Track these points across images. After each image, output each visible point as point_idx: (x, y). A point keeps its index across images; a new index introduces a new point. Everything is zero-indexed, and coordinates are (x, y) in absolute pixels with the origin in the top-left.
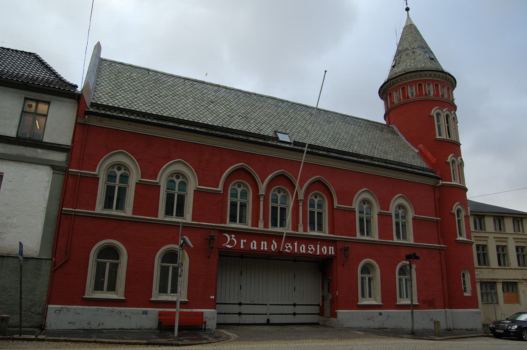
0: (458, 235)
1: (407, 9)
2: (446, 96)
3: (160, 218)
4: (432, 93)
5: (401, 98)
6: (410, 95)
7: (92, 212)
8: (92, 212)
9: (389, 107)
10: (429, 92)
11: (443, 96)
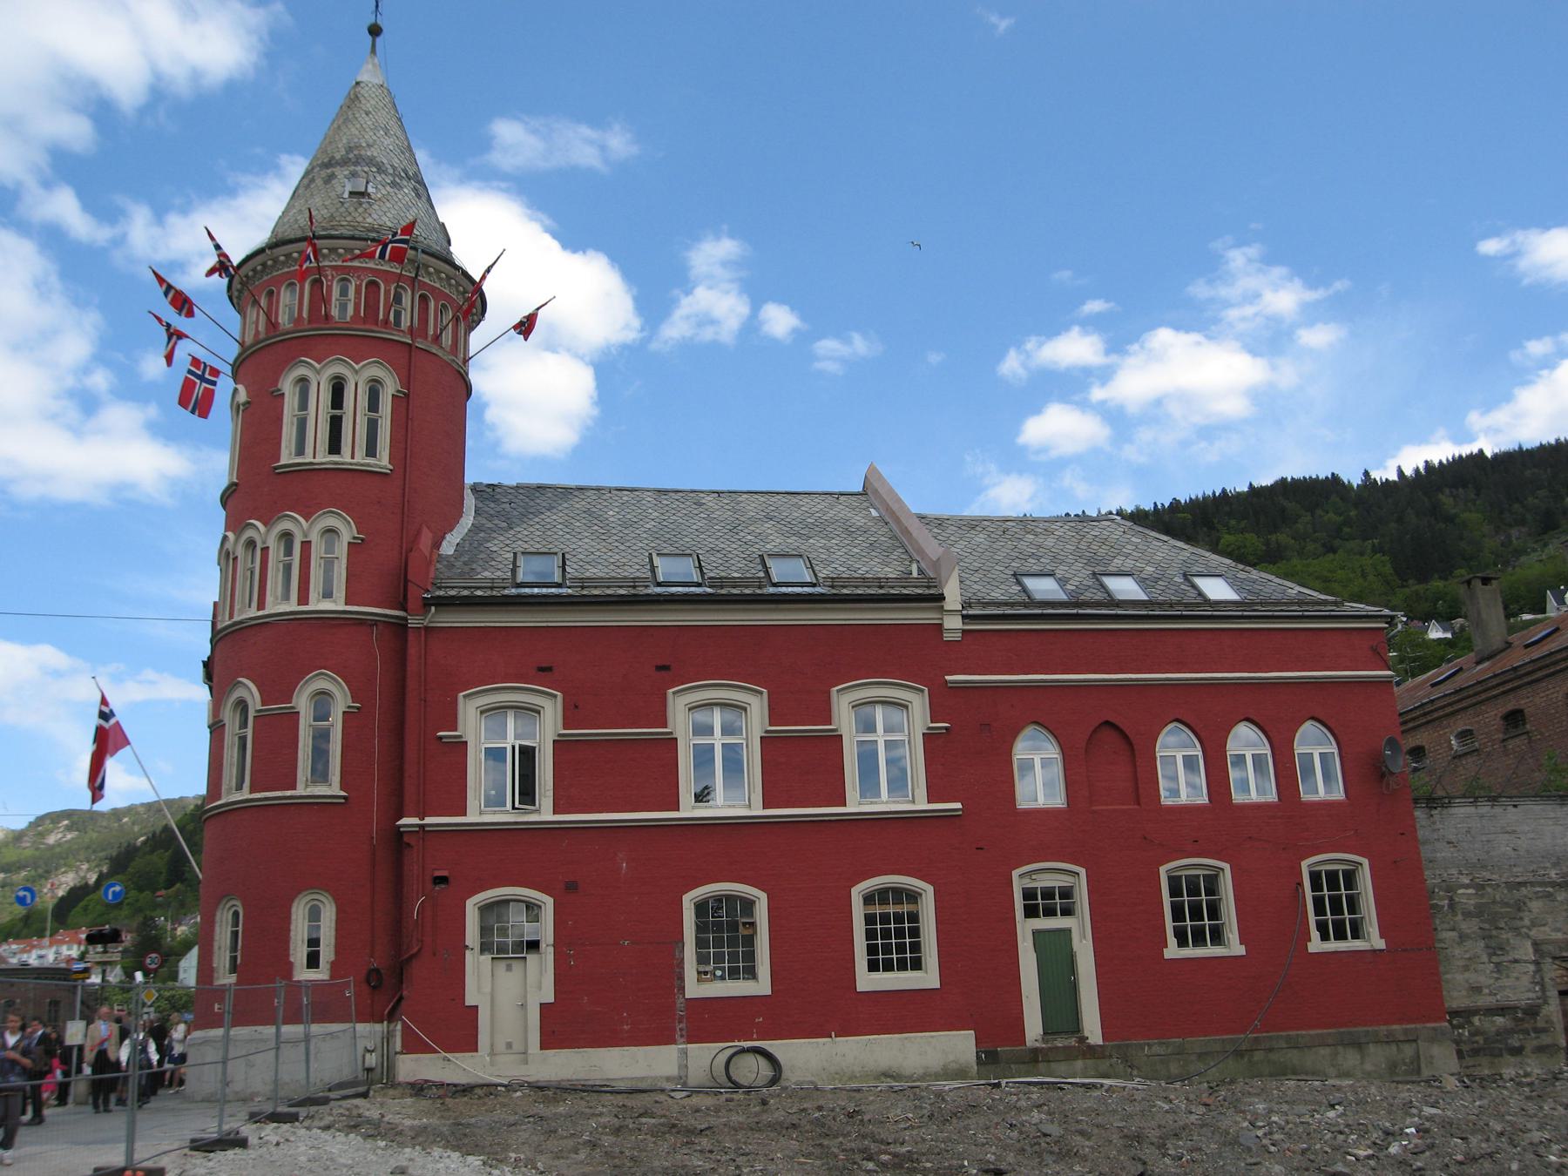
0: (1315, 934)
1: (375, 31)
2: (447, 339)
3: (300, 791)
4: (405, 322)
5: (305, 315)
6: (335, 312)
7: (289, 793)
8: (289, 793)
9: (262, 336)
10: (398, 315)
11: (437, 338)
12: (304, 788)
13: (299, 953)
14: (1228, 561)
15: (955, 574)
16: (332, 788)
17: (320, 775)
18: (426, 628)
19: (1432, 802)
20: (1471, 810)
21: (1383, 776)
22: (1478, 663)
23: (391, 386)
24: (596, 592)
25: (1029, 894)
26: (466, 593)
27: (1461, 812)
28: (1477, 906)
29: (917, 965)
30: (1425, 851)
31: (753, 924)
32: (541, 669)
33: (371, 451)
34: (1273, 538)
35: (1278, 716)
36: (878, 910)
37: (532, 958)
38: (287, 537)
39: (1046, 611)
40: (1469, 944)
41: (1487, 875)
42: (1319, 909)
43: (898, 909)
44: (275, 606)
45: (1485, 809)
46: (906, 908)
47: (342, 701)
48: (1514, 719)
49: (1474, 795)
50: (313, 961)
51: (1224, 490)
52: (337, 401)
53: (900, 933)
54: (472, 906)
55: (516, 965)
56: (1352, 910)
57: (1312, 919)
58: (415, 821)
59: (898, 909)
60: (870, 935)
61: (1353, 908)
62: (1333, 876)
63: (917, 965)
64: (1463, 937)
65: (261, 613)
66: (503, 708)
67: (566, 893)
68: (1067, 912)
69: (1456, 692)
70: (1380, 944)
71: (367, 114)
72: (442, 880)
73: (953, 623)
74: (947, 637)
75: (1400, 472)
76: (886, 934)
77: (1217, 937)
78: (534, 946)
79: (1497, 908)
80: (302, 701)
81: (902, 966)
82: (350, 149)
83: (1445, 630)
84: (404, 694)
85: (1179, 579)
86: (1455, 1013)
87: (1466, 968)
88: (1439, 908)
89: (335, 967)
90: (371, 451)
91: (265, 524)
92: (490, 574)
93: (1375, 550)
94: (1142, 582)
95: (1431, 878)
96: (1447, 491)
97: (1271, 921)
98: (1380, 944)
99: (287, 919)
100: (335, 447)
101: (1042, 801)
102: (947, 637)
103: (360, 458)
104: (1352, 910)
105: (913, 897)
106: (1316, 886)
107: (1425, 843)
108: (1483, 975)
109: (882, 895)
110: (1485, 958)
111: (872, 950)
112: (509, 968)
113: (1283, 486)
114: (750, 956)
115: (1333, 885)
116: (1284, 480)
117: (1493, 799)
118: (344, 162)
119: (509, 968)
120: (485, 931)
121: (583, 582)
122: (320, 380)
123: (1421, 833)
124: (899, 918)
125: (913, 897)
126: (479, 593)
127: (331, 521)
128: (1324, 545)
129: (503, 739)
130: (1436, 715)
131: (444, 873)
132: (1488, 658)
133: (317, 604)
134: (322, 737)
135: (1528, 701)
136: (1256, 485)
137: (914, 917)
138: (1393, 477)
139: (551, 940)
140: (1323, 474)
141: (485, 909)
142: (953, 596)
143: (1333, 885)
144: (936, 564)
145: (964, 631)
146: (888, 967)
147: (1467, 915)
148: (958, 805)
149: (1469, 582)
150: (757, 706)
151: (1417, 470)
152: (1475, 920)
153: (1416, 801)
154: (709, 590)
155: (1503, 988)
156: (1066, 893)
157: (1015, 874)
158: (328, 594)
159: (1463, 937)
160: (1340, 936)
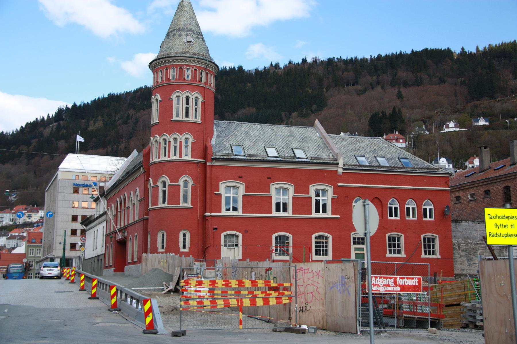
0: (423, 253)
7: (178, 206)
8: (178, 206)
11: (210, 85)
12: (182, 205)
13: (181, 245)
14: (410, 154)
15: (342, 158)
16: (189, 205)
17: (185, 201)
18: (212, 166)
19: (457, 221)
20: (467, 224)
21: (444, 215)
22: (480, 172)
23: (201, 99)
24: (254, 158)
25: (354, 239)
26: (222, 157)
27: (464, 224)
28: (466, 248)
29: (326, 254)
30: (453, 234)
31: (289, 243)
32: (240, 177)
33: (196, 117)
34: (419, 75)
35: (419, 197)
36: (318, 240)
37: (236, 248)
38: (175, 139)
39: (361, 167)
40: (462, 258)
41: (469, 241)
42: (425, 247)
43: (323, 241)
44: (173, 158)
45: (471, 224)
46: (324, 241)
47: (191, 183)
48: (487, 192)
49: (467, 221)
50: (184, 247)
51: (401, 52)
52: (187, 103)
53: (323, 247)
54: (223, 235)
55: (233, 250)
56: (433, 248)
57: (423, 249)
58: (209, 214)
59: (323, 241)
60: (316, 247)
61: (433, 247)
62: (429, 239)
63: (326, 254)
64: (461, 256)
65: (169, 159)
66: (230, 186)
67: (245, 233)
68: (363, 244)
69: (471, 182)
70: (439, 257)
71: (187, 13)
72: (216, 229)
73: (340, 171)
74: (339, 174)
76: (320, 247)
77: (399, 252)
78: (237, 245)
79: (471, 249)
80: (181, 183)
81: (323, 255)
82: (184, 26)
83: (486, 121)
84: (206, 182)
85: (397, 159)
86: (457, 275)
87: (461, 264)
88: (455, 248)
89: (190, 248)
90: (196, 117)
91: (169, 135)
92: (226, 152)
93: (462, 83)
94: (388, 160)
95: (454, 241)
96: (497, 59)
98: (439, 257)
99: (178, 236)
100: (187, 116)
102: (339, 174)
103: (194, 119)
104: (433, 248)
105: (327, 238)
106: (425, 241)
107: (454, 231)
108: (466, 267)
110: (466, 262)
111: (316, 250)
112: (230, 251)
113: (426, 52)
115: (429, 241)
116: (427, 49)
117: (473, 222)
118: (183, 30)
119: (230, 251)
120: (225, 241)
121: (250, 156)
122: (183, 96)
123: (453, 229)
125: (327, 238)
126: (225, 157)
127: (187, 136)
128: (440, 79)
129: (231, 194)
131: (216, 227)
132: (483, 171)
133: (184, 158)
134: (186, 192)
135: (491, 188)
136: (414, 50)
137: (326, 243)
138: (474, 51)
139: (241, 244)
140: (444, 47)
141: (225, 236)
142: (341, 163)
143: (429, 241)
144: (337, 155)
146: (320, 254)
147: (463, 251)
148: (339, 216)
149: (480, 148)
150: (291, 189)
151: (485, 48)
153: (452, 221)
154: (282, 159)
155: (470, 270)
157: (351, 234)
158: (186, 155)
159: (461, 256)
160: (429, 254)
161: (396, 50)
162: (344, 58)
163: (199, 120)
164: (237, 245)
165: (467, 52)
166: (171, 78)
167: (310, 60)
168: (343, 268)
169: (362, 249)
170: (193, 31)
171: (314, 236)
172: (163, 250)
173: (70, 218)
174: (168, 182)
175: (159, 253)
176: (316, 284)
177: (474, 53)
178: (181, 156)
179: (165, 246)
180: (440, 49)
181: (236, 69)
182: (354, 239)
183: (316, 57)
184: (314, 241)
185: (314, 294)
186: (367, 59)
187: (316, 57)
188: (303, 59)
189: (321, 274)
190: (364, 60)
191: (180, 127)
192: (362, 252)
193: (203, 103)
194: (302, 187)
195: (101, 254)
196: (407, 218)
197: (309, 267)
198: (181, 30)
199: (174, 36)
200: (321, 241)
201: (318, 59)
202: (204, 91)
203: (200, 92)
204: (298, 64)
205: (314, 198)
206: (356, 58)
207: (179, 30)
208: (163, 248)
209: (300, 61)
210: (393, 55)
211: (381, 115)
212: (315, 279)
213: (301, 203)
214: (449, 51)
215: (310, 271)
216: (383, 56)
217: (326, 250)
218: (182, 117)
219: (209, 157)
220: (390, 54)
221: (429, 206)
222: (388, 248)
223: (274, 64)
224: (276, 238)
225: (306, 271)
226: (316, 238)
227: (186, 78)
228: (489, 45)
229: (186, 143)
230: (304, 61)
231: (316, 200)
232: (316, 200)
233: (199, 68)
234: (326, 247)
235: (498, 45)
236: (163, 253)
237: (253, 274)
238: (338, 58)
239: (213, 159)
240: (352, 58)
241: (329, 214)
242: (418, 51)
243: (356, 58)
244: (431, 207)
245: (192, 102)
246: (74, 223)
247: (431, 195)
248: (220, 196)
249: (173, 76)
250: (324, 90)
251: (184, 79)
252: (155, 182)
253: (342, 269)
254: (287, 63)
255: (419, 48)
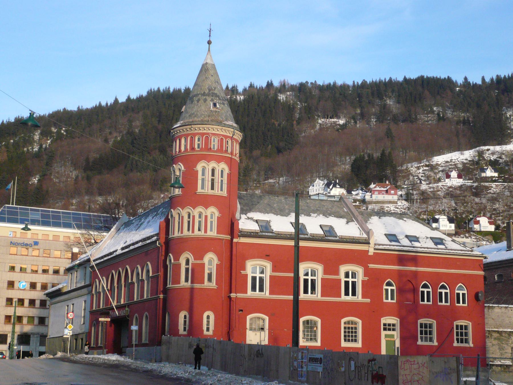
0: (456, 341)
4: (229, 151)
17: (210, 279)
29: (356, 341)
33: (222, 190)
37: (262, 333)
42: (457, 335)
50: (208, 329)
51: (391, 79)
52: (213, 175)
54: (249, 317)
57: (455, 337)
60: (345, 332)
64: (493, 345)
68: (394, 330)
71: (212, 76)
74: (370, 254)
75: (483, 79)
77: (431, 340)
78: (262, 329)
83: (495, 172)
89: (214, 331)
90: (222, 190)
97: (445, 335)
100: (213, 188)
101: (294, 243)
102: (370, 254)
106: (457, 329)
109: (348, 323)
111: (345, 336)
114: (315, 336)
116: (422, 77)
118: (208, 95)
120: (251, 324)
124: (352, 328)
130: (492, 267)
136: (407, 77)
137: (356, 328)
138: (479, 82)
139: (267, 328)
140: (443, 75)
145: (374, 253)
146: (349, 341)
148: (369, 300)
151: (492, 79)
152: (497, 341)
156: (394, 325)
159: (493, 345)
160: (462, 342)
161: (385, 76)
162: (320, 83)
163: (225, 193)
164: (262, 329)
165: (471, 82)
166: (196, 146)
167: (276, 84)
168: (446, 360)
169: (393, 336)
170: (218, 96)
171: (343, 321)
172: (185, 333)
173: (6, 285)
174: (192, 260)
175: (180, 336)
176: (421, 373)
177: (480, 85)
178: (206, 231)
179: (187, 329)
180: (438, 77)
181: (183, 91)
182: (385, 325)
183: (284, 81)
184: (343, 326)
185: (419, 382)
186: (348, 86)
187: (284, 81)
188: (268, 82)
189: (425, 365)
190: (344, 87)
191: (206, 201)
192: (392, 339)
193: (229, 175)
194: (331, 268)
195: (81, 332)
196: (439, 304)
197: (416, 360)
198: (206, 95)
199: (198, 101)
200: (350, 326)
201: (286, 83)
202: (230, 162)
203: (226, 163)
204: (261, 89)
205: (343, 279)
206: (335, 84)
207: (204, 94)
208: (185, 330)
209: (264, 85)
210: (381, 81)
211: (367, 158)
212: (421, 369)
213: (331, 287)
214: (449, 80)
215: (416, 362)
216: (368, 82)
217: (356, 336)
218: (208, 190)
219: (236, 232)
220: (378, 80)
221: (462, 291)
222: (419, 336)
223: (230, 87)
224: (304, 322)
225: (412, 363)
226: (345, 323)
227: (212, 147)
228: (497, 76)
229: (212, 218)
230: (270, 85)
231: (345, 281)
232: (345, 281)
233: (226, 137)
234: (356, 332)
235: (507, 76)
236: (184, 335)
237: (352, 363)
238: (312, 83)
239: (239, 236)
240: (330, 84)
241: (359, 298)
242: (412, 78)
243: (335, 84)
244: (464, 292)
245: (217, 173)
246: (10, 291)
247: (466, 280)
248: (246, 276)
249: (199, 145)
250: (295, 122)
251: (210, 148)
252: (177, 258)
253: (445, 362)
254: (247, 86)
255: (413, 75)
